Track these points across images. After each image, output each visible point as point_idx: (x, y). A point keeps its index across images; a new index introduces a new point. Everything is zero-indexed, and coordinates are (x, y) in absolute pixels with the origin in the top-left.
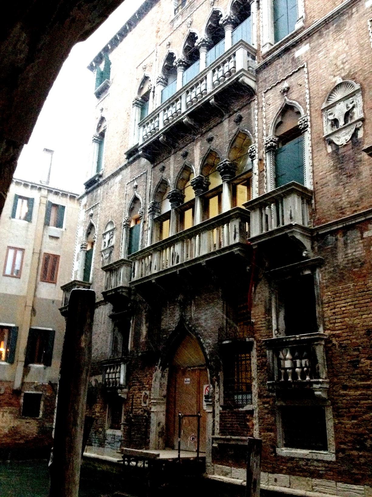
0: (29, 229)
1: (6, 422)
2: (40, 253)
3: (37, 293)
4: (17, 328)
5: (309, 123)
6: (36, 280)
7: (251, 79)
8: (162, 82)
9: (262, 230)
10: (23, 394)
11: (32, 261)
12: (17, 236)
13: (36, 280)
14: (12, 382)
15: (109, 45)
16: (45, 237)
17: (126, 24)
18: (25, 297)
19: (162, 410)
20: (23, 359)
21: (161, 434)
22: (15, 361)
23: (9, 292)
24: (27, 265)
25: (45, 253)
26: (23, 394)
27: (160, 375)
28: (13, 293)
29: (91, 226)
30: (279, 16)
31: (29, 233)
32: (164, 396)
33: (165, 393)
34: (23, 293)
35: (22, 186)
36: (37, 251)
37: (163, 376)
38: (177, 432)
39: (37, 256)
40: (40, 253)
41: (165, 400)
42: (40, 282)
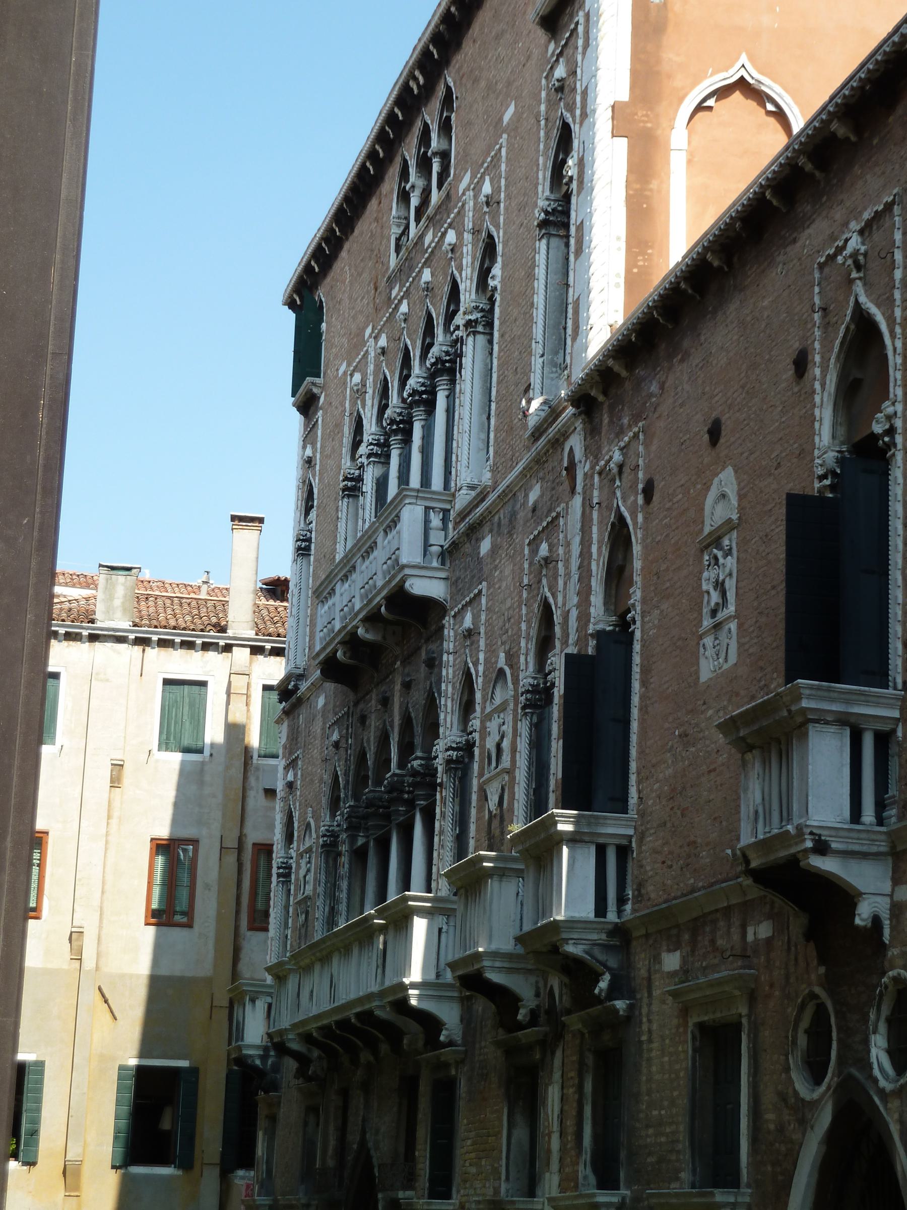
0: (207, 778)
2: (240, 848)
3: (242, 967)
4: (193, 1072)
5: (476, 736)
6: (237, 928)
9: (269, 1028)
11: (220, 872)
13: (237, 928)
15: (396, 110)
17: (331, 222)
18: (208, 981)
20: (217, 1159)
22: (197, 1164)
24: (207, 887)
25: (254, 844)
28: (178, 973)
29: (547, 613)
30: (194, 746)
34: (205, 969)
36: (232, 843)
39: (231, 859)
40: (240, 848)
42: (249, 933)
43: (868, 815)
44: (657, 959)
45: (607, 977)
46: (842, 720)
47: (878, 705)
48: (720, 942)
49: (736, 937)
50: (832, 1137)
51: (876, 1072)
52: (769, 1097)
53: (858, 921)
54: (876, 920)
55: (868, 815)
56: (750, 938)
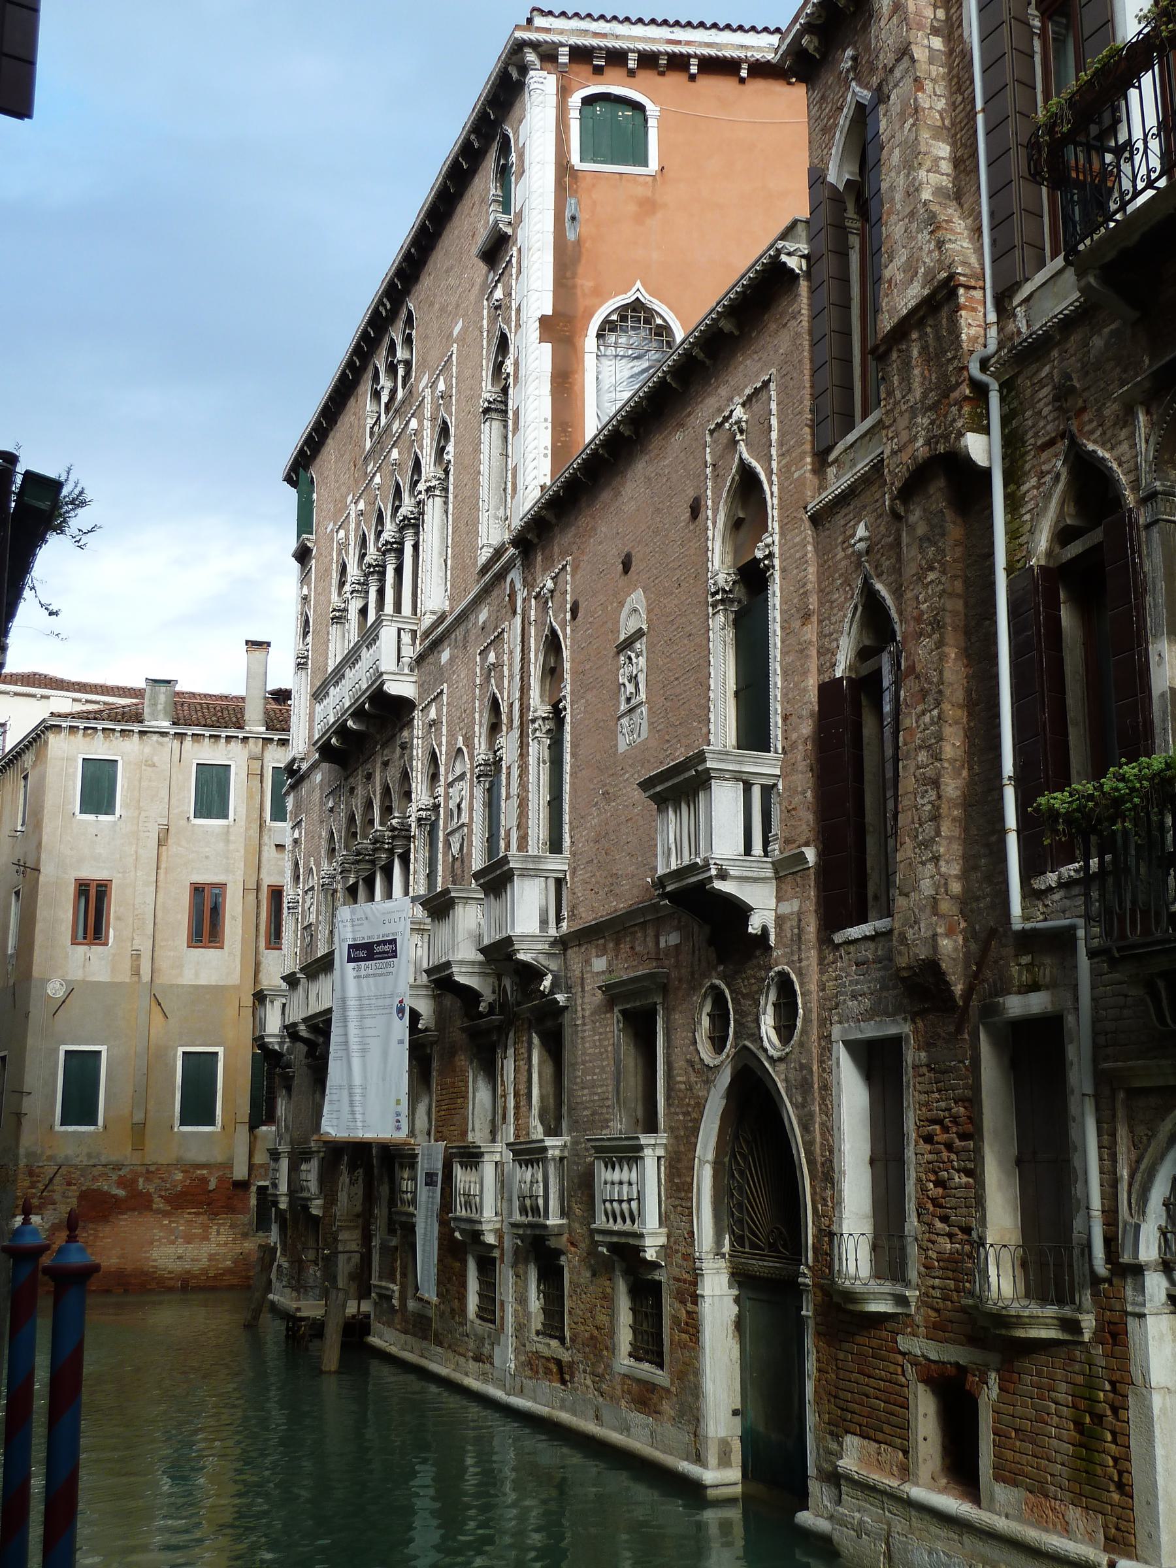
0: (232, 838)
1: (226, 1244)
5: (441, 799)
7: (16, 694)
8: (358, 591)
10: (254, 1189)
12: (207, 857)
14: (228, 1165)
16: (265, 849)
19: (354, 1237)
21: (352, 1277)
23: (202, 981)
26: (254, 1189)
27: (347, 1180)
31: (232, 847)
32: (358, 1216)
33: (359, 1209)
35: (207, 740)
37: (352, 1183)
38: (632, 1241)
39: (252, 897)
41: (360, 1221)
43: (757, 849)
44: (588, 962)
45: (550, 977)
46: (738, 777)
47: (764, 765)
48: (638, 949)
49: (651, 944)
50: (732, 1092)
51: (766, 1044)
52: (680, 1063)
53: (750, 930)
54: (765, 929)
55: (757, 849)
56: (662, 945)
